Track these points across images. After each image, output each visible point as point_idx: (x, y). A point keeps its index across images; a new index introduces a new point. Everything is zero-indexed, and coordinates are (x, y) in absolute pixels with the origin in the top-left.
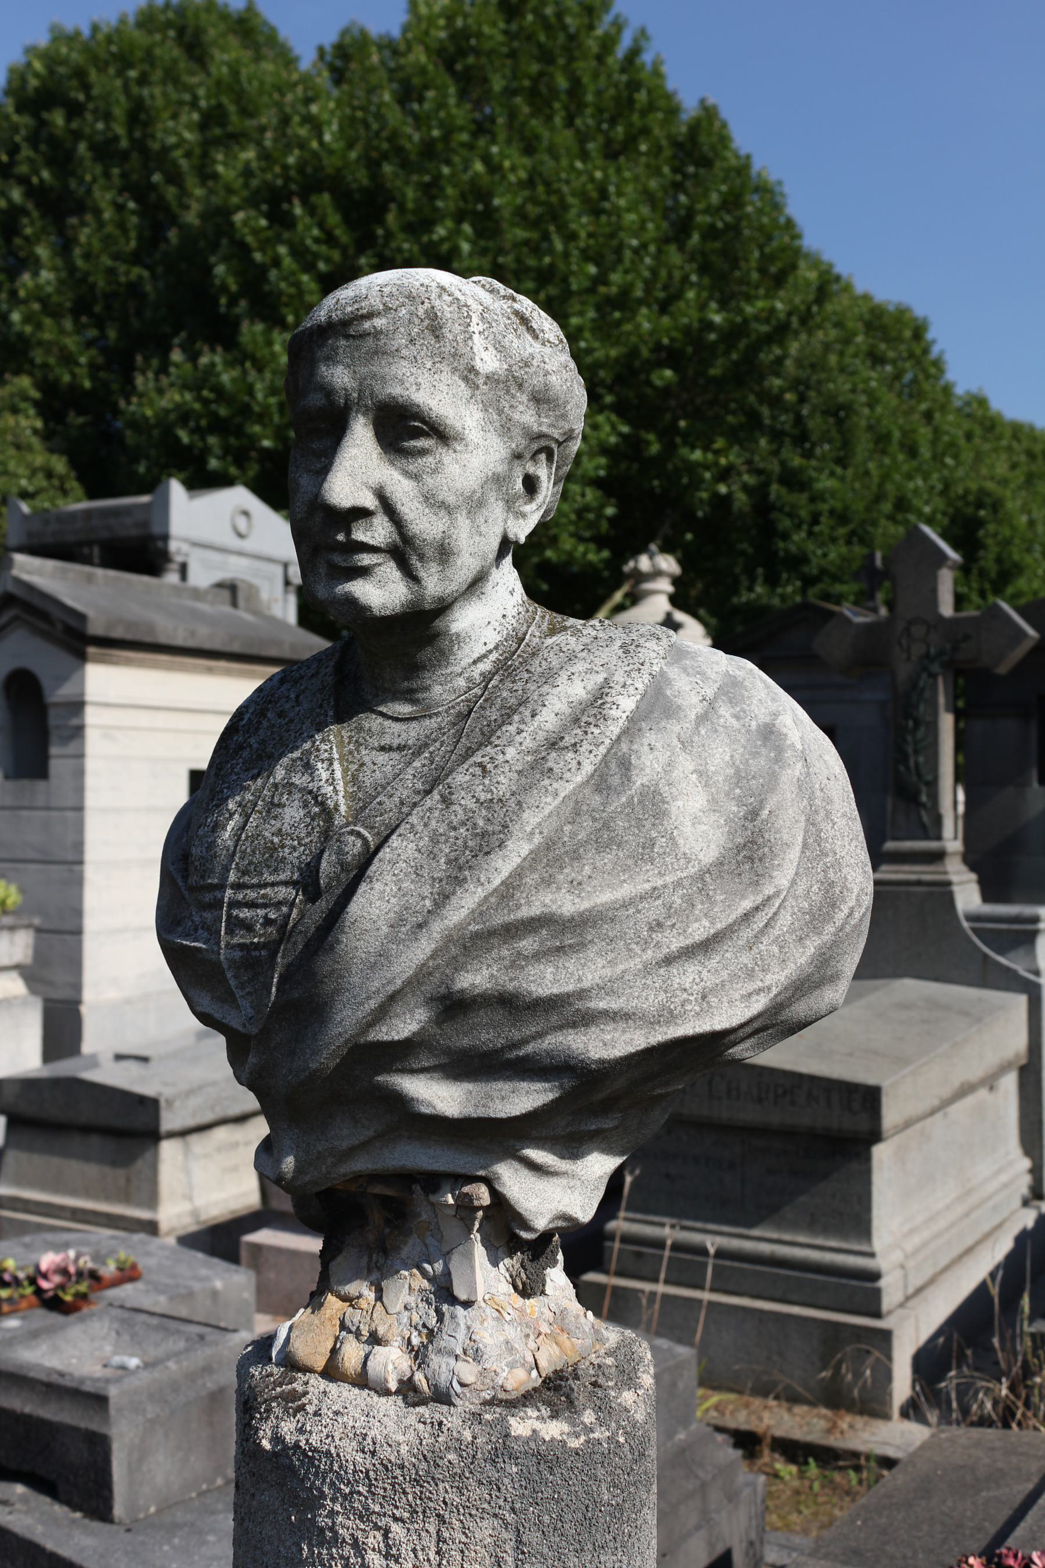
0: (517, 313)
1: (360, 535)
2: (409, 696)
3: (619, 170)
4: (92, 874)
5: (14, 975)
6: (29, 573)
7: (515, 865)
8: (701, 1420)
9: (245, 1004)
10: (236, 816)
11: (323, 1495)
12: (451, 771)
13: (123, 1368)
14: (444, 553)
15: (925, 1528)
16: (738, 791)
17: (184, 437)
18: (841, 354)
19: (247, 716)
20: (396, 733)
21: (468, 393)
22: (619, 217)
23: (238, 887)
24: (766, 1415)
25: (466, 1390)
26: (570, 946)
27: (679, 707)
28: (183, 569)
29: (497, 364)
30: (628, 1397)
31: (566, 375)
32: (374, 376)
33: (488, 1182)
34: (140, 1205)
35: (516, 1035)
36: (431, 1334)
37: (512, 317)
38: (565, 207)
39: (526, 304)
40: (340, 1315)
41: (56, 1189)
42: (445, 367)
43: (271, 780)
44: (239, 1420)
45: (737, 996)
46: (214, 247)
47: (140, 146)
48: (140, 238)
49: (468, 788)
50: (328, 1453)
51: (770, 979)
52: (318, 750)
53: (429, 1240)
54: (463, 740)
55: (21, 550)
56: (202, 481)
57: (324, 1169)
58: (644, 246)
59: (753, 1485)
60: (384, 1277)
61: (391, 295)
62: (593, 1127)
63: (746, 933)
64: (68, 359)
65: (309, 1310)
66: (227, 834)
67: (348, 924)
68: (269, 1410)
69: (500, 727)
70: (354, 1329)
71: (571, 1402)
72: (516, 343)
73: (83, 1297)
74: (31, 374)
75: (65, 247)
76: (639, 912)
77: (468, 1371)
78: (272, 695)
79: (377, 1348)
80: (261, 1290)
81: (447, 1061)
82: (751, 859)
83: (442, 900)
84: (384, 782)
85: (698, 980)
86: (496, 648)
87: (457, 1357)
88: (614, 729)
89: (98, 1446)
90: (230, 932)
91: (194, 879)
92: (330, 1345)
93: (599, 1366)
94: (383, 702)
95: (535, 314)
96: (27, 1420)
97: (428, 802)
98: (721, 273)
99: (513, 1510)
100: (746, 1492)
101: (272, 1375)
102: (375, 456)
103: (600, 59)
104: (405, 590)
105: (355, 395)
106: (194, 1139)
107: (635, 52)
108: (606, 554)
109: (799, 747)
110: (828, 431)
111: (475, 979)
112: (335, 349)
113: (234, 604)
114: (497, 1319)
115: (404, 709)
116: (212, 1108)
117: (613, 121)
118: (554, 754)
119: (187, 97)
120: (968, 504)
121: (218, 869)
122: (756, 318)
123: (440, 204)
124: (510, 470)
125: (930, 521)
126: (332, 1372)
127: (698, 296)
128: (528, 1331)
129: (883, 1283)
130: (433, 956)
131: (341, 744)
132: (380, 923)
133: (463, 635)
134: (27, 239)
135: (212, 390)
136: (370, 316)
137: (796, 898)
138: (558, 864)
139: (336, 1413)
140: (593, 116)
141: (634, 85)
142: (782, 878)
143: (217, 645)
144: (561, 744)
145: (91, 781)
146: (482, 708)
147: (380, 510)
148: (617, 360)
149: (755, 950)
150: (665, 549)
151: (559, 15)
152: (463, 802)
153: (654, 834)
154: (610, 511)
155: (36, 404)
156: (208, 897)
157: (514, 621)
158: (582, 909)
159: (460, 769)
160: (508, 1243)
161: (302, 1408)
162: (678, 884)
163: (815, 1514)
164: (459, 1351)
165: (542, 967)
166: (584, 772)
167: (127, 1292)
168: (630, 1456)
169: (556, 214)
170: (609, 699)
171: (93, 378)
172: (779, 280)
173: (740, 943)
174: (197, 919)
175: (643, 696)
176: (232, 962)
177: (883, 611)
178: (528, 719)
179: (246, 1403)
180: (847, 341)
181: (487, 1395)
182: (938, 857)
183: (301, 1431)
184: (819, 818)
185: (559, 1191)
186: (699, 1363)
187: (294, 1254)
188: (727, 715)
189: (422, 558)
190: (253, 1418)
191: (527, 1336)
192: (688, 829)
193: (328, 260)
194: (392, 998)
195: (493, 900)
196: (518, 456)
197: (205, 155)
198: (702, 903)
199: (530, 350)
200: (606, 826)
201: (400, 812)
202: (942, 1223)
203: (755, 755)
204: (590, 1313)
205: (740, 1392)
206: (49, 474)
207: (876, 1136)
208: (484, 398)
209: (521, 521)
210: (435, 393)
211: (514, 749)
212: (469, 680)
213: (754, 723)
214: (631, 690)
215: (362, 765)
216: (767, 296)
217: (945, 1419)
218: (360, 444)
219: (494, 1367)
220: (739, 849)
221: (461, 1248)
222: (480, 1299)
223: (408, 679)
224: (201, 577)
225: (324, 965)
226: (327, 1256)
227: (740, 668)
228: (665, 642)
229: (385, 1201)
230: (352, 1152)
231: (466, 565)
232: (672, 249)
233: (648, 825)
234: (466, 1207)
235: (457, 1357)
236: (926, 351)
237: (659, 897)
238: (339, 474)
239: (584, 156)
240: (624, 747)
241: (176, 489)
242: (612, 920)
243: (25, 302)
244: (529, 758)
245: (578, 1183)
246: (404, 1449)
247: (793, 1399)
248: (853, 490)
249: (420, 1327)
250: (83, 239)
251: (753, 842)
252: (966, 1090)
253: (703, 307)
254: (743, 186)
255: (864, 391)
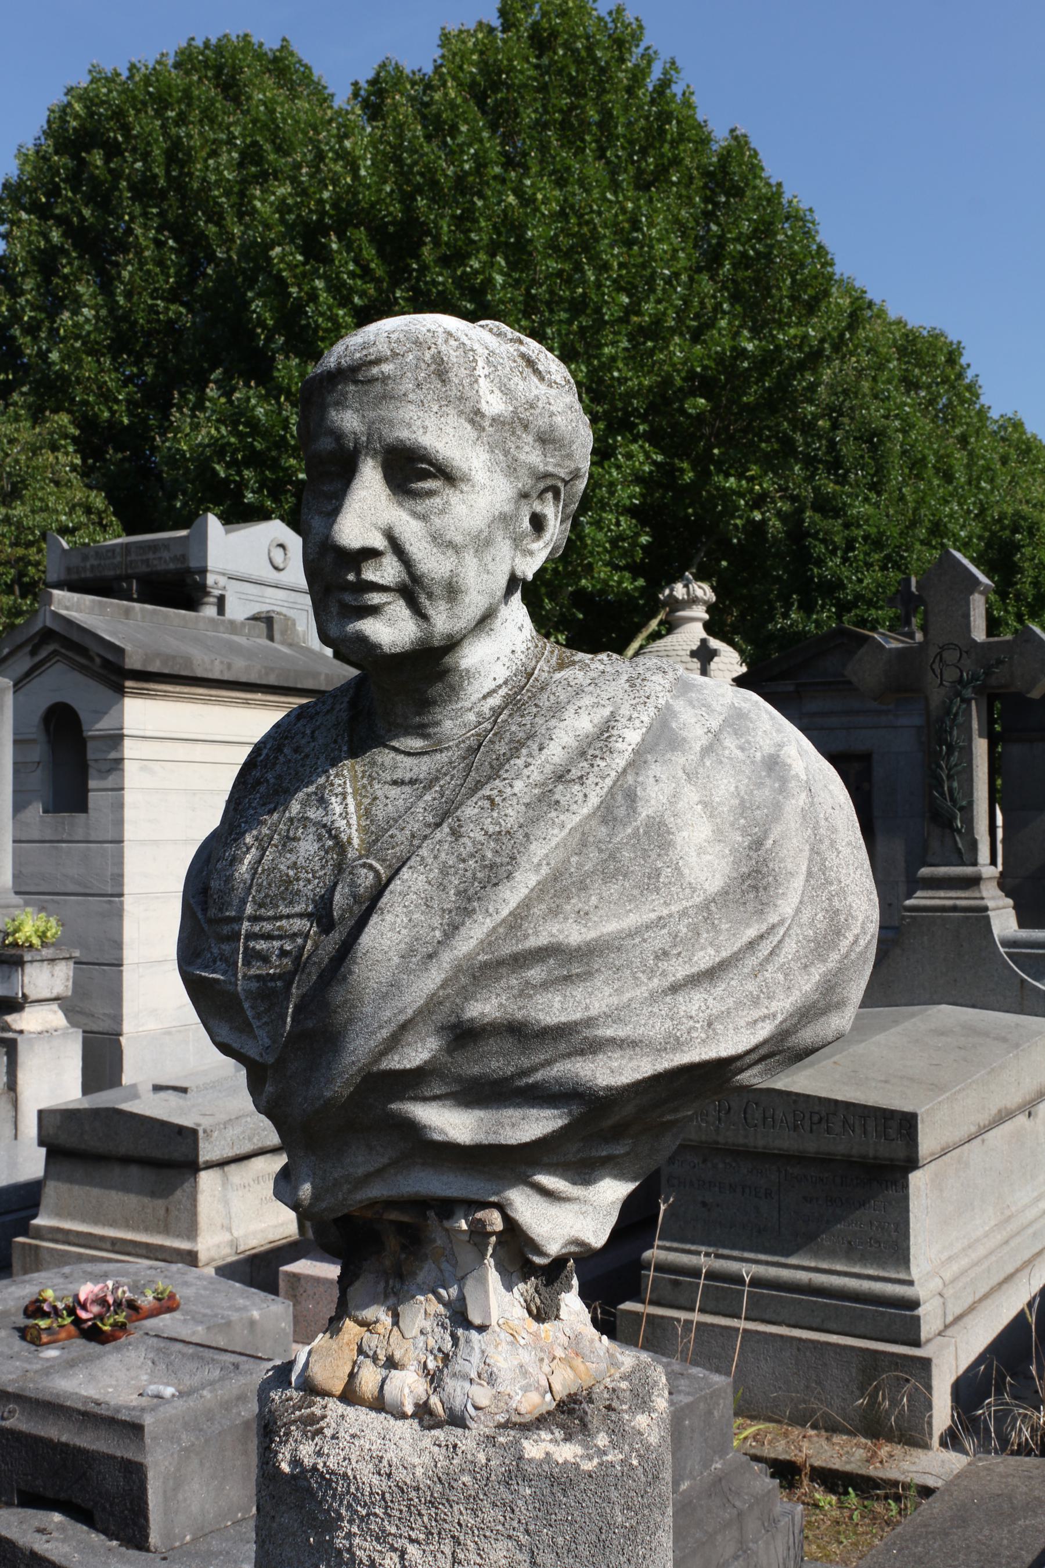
0: (523, 356)
1: (370, 574)
2: (421, 731)
3: (651, 200)
4: (130, 905)
5: (55, 1006)
6: (67, 608)
7: (522, 896)
8: (738, 1450)
9: (262, 1033)
10: (253, 850)
11: (340, 1517)
12: (461, 804)
13: (159, 1397)
14: (452, 591)
15: (961, 1557)
16: (742, 821)
17: (221, 471)
18: (875, 379)
19: (265, 752)
20: (408, 767)
21: (474, 435)
22: (651, 247)
23: (255, 919)
24: (805, 1444)
25: (480, 1413)
26: (577, 975)
27: (684, 739)
28: (221, 601)
29: (502, 407)
30: (641, 1420)
31: (571, 416)
32: (382, 420)
33: (500, 1207)
34: (178, 1236)
35: (526, 1063)
36: (446, 1358)
37: (519, 360)
38: (597, 238)
39: (532, 347)
40: (357, 1340)
41: (96, 1222)
42: (450, 410)
43: (287, 815)
44: (260, 1443)
45: (742, 1023)
46: (251, 282)
47: (179, 186)
48: (177, 275)
49: (477, 821)
50: (345, 1476)
51: (775, 1006)
52: (332, 785)
53: (444, 1266)
54: (473, 774)
55: (59, 586)
56: (238, 515)
57: (340, 1196)
58: (676, 275)
59: (792, 1514)
60: (400, 1302)
61: (398, 341)
62: (604, 1153)
63: (751, 961)
64: (107, 397)
65: (328, 1335)
66: (244, 868)
67: (359, 954)
68: (288, 1434)
69: (508, 760)
70: (371, 1353)
71: (584, 1425)
72: (522, 385)
73: (122, 1327)
74: (69, 412)
75: (106, 285)
76: (645, 941)
77: (482, 1395)
78: (289, 731)
79: (393, 1372)
80: (297, 1320)
81: (458, 1088)
82: (755, 888)
83: (452, 930)
84: (396, 815)
85: (703, 1008)
86: (506, 683)
87: (471, 1380)
88: (620, 762)
89: (134, 1474)
90: (247, 963)
91: (212, 912)
92: (347, 1369)
93: (614, 1390)
94: (396, 737)
95: (542, 357)
96: (64, 1448)
97: (438, 835)
98: (752, 300)
99: (527, 1532)
100: (784, 1522)
101: (291, 1399)
102: (383, 498)
103: (630, 91)
104: (414, 628)
105: (364, 439)
106: (232, 1169)
107: (665, 84)
108: (641, 582)
109: (804, 777)
110: (862, 457)
111: (485, 1008)
112: (344, 394)
113: (271, 638)
114: (512, 1343)
115: (416, 743)
116: (250, 1139)
117: (644, 152)
118: (561, 787)
119: (223, 136)
120: (1003, 528)
121: (236, 902)
122: (789, 345)
123: (474, 236)
124: (517, 509)
125: (965, 546)
126: (349, 1396)
127: (730, 323)
128: (542, 1355)
129: (921, 1311)
130: (443, 986)
131: (354, 779)
132: (391, 954)
133: (473, 670)
134: (65, 278)
135: (246, 425)
136: (378, 361)
137: (801, 926)
138: (565, 894)
139: (353, 1436)
140: (623, 148)
141: (665, 117)
142: (787, 907)
143: (253, 678)
144: (568, 777)
145: (128, 814)
146: (491, 742)
147: (389, 550)
148: (650, 388)
149: (760, 978)
150: (698, 578)
151: (590, 49)
152: (472, 835)
153: (659, 864)
154: (644, 539)
155: (75, 440)
156: (226, 929)
157: (523, 657)
158: (589, 938)
159: (469, 803)
160: (522, 1268)
161: (320, 1431)
162: (684, 913)
163: (855, 1544)
164: (473, 1375)
165: (550, 995)
166: (590, 804)
167: (165, 1322)
168: (643, 1479)
169: (587, 245)
170: (615, 732)
171: (130, 414)
172: (812, 307)
173: (746, 970)
174: (215, 951)
175: (649, 729)
176: (248, 992)
177: (919, 636)
178: (536, 753)
179: (266, 1426)
180: (881, 367)
181: (501, 1418)
182: (975, 881)
183: (319, 1454)
184: (824, 847)
185: (577, 1215)
186: (735, 1392)
187: (317, 1280)
188: (732, 747)
189: (430, 596)
190: (272, 1441)
191: (542, 1360)
192: (693, 859)
193: (363, 294)
194: (404, 1027)
195: (501, 930)
196: (524, 496)
197: (242, 194)
198: (708, 932)
199: (536, 392)
200: (612, 857)
201: (411, 845)
202: (981, 1251)
203: (760, 785)
204: (605, 1338)
205: (778, 1422)
206: (88, 510)
207: (912, 1163)
208: (490, 439)
209: (529, 558)
210: (441, 435)
211: (521, 783)
212: (479, 714)
213: (758, 755)
214: (637, 723)
215: (375, 799)
216: (799, 324)
217: (984, 1447)
218: (370, 484)
219: (508, 1391)
220: (744, 878)
221: (475, 1273)
222: (494, 1323)
223: (420, 715)
224: (237, 610)
225: (337, 995)
226: (344, 1281)
227: (745, 700)
228: (671, 675)
229: (401, 1228)
230: (368, 1178)
231: (473, 604)
232: (705, 276)
233: (654, 856)
234: (479, 1233)
235: (471, 1380)
236: (960, 376)
237: (664, 926)
238: (348, 516)
239: (615, 186)
240: (630, 779)
241: (213, 523)
242: (619, 950)
243: (63, 340)
244: (536, 791)
245: (591, 1208)
246: (419, 1472)
247: (832, 1428)
248: (887, 516)
249: (435, 1351)
250: (125, 274)
251: (758, 872)
252: (1003, 1117)
253: (736, 335)
254: (774, 213)
255: (896, 416)
